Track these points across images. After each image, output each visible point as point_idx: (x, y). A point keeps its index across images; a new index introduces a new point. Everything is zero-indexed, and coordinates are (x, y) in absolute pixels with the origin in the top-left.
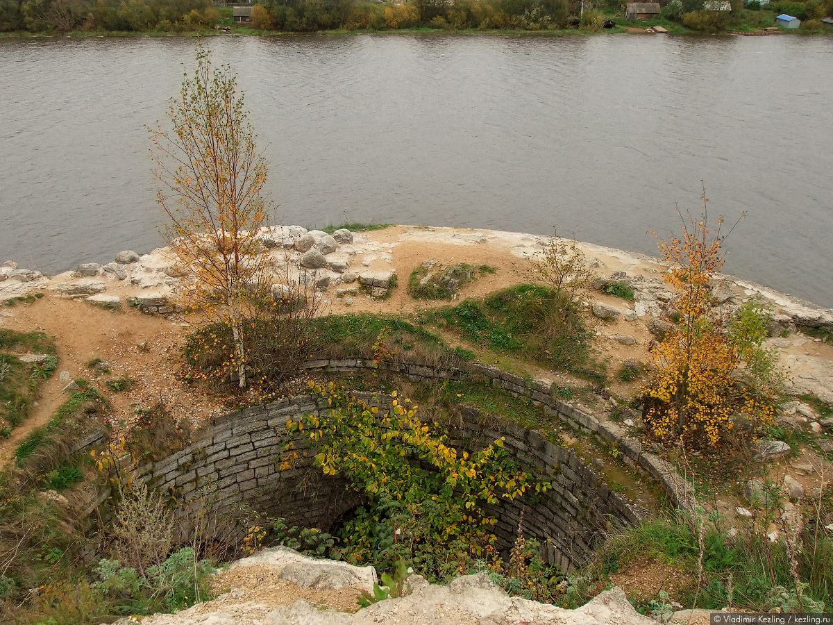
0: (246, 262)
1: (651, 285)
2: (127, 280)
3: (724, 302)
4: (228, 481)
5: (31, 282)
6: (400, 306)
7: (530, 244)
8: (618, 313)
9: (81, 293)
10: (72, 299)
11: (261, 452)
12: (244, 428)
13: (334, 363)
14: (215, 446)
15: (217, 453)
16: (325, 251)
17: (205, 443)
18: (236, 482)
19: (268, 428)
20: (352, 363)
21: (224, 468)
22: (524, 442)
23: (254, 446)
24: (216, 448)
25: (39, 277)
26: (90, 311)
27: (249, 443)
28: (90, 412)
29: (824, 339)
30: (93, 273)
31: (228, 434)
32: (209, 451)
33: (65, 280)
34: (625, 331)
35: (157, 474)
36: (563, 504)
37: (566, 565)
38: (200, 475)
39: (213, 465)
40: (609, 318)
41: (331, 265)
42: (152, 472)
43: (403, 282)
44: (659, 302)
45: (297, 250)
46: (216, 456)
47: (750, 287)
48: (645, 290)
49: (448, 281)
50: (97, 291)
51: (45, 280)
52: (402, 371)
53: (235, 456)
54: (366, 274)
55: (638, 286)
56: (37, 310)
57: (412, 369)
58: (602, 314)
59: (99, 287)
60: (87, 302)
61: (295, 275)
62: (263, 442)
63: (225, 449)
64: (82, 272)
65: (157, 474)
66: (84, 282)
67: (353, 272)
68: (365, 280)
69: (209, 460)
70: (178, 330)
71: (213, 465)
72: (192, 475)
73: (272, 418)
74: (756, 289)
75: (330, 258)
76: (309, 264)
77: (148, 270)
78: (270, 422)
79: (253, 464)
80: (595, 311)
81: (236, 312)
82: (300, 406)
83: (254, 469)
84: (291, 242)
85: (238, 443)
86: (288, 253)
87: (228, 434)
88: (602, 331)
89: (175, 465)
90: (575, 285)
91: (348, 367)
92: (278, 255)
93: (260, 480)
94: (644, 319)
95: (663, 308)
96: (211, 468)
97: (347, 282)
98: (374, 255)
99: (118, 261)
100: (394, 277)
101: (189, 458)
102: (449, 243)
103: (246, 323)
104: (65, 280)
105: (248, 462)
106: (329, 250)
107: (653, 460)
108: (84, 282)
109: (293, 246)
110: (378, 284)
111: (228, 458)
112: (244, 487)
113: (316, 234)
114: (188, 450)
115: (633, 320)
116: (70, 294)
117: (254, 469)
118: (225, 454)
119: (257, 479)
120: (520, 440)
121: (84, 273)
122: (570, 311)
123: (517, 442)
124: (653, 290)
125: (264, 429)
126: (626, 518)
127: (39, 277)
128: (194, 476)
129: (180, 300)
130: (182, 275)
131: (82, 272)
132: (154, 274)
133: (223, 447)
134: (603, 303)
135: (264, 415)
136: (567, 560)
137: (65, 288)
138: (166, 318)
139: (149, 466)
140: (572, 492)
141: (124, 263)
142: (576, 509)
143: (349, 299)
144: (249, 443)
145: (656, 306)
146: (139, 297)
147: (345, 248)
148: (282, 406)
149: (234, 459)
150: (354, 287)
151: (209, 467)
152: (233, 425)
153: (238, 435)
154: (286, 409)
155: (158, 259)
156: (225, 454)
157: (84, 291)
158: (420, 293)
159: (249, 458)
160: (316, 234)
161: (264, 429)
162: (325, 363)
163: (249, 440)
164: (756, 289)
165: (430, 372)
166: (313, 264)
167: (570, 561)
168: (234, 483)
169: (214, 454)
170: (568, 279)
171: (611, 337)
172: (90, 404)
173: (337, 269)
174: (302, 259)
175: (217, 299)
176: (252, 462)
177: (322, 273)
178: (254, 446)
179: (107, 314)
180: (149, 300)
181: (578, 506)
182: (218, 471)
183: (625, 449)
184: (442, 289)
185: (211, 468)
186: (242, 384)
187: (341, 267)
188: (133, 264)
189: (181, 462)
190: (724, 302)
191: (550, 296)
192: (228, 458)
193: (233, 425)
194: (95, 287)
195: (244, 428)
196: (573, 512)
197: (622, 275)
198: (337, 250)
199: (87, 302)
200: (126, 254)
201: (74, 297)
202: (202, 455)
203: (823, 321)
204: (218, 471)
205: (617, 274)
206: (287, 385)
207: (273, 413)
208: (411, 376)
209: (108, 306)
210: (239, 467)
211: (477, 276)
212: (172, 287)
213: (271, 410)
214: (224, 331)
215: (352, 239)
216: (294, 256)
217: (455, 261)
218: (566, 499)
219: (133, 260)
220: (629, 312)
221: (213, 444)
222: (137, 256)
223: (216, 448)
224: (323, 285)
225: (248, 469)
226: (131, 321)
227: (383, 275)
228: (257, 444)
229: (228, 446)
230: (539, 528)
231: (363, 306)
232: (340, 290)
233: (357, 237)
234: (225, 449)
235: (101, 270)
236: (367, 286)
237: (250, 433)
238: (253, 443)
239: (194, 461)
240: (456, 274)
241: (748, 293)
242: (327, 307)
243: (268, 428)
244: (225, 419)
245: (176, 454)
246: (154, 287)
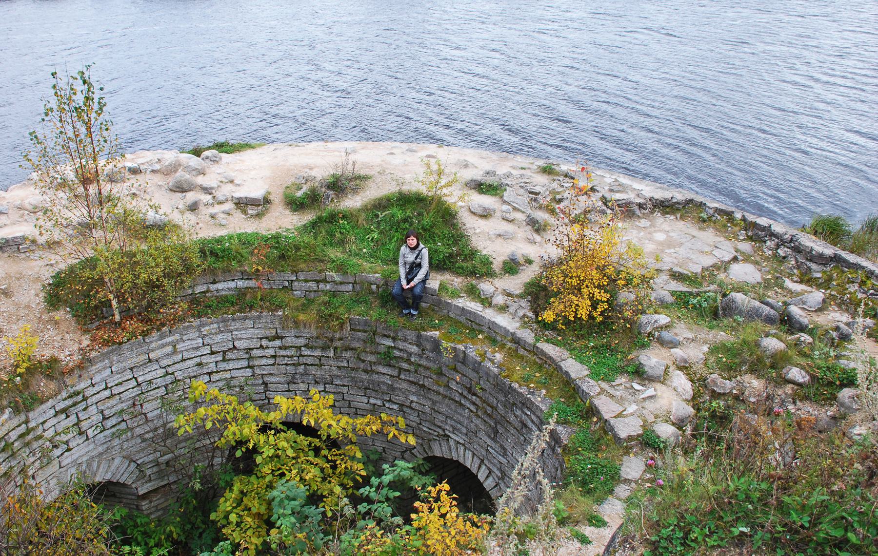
0: (118, 189)
4: (113, 421)
6: (283, 222)
12: (124, 364)
16: (194, 173)
18: (123, 420)
21: (108, 408)
22: (417, 345)
23: (137, 381)
24: (97, 388)
26: (434, 154)
29: (678, 216)
36: (463, 402)
37: (470, 458)
38: (82, 418)
39: (94, 407)
43: (277, 198)
46: (97, 396)
47: (607, 175)
53: (119, 394)
55: (509, 183)
58: (479, 211)
62: (147, 376)
67: (227, 191)
69: (89, 401)
70: (42, 268)
71: (94, 407)
73: (153, 351)
75: (200, 180)
76: (178, 187)
78: (152, 355)
81: (107, 242)
89: (52, 412)
93: (148, 415)
96: (93, 410)
98: (255, 172)
107: (550, 349)
118: (107, 393)
123: (410, 346)
124: (523, 185)
126: (528, 408)
128: (76, 420)
133: (104, 386)
136: (470, 453)
149: (118, 397)
151: (90, 409)
156: (107, 393)
159: (134, 395)
163: (131, 376)
167: (474, 454)
168: (121, 422)
177: (191, 197)
178: (137, 381)
183: (516, 341)
187: (212, 188)
195: (124, 364)
203: (674, 200)
207: (153, 345)
213: (151, 342)
215: (221, 159)
223: (97, 388)
227: (257, 193)
228: (140, 379)
229: (109, 385)
230: (440, 427)
231: (241, 225)
236: (242, 204)
237: (131, 369)
238: (136, 379)
242: (200, 229)
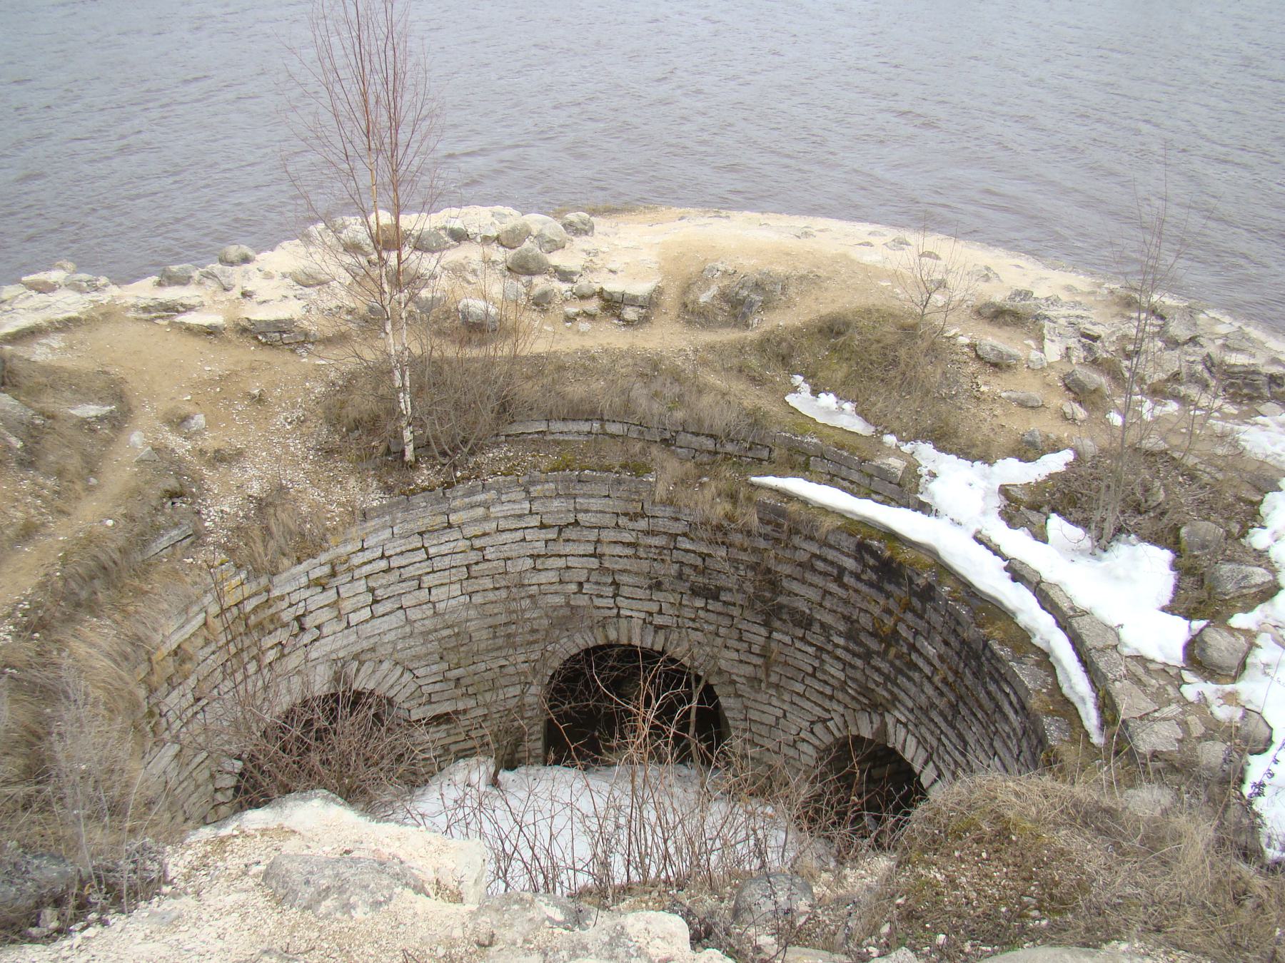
1: (1073, 312)
2: (236, 293)
3: (1185, 343)
5: (95, 294)
7: (884, 240)
8: (1017, 359)
9: (166, 311)
10: (152, 320)
11: (438, 564)
13: (557, 426)
14: (367, 553)
15: (370, 562)
16: (548, 246)
17: (350, 548)
19: (450, 526)
20: (585, 427)
22: (856, 559)
23: (427, 553)
24: (368, 555)
25: (105, 286)
27: (419, 549)
28: (173, 495)
30: (183, 281)
31: (387, 534)
32: (356, 560)
33: (145, 291)
34: (1031, 388)
35: (276, 593)
37: (913, 748)
38: (343, 595)
39: (363, 582)
40: (999, 365)
41: (557, 269)
42: (268, 591)
43: (670, 300)
44: (1083, 340)
45: (502, 245)
47: (1227, 319)
48: (1063, 321)
49: (745, 298)
50: (189, 308)
51: (114, 290)
52: (664, 441)
54: (614, 286)
56: (106, 333)
57: (684, 439)
58: (992, 357)
59: (194, 301)
60: (172, 324)
61: (496, 286)
62: (443, 547)
63: (383, 557)
64: (169, 278)
65: (276, 593)
66: (171, 294)
67: (583, 283)
68: (610, 294)
69: (357, 574)
71: (363, 582)
72: (331, 595)
74: (1237, 324)
75: (556, 259)
77: (268, 276)
78: (581, 517)
79: (428, 581)
80: (980, 352)
82: (499, 492)
83: (430, 589)
84: (493, 233)
85: (404, 548)
86: (486, 249)
87: (387, 534)
88: (990, 385)
89: (304, 580)
90: (947, 308)
91: (579, 433)
92: (470, 254)
94: (1059, 367)
95: (1089, 349)
97: (583, 297)
98: (630, 253)
99: (224, 261)
100: (659, 291)
101: (326, 570)
102: (747, 239)
103: (415, 363)
104: (145, 291)
105: (419, 578)
106: (556, 246)
108: (171, 294)
109: (497, 239)
110: (632, 301)
111: (389, 570)
112: (414, 614)
113: (536, 221)
114: (323, 557)
115: (1040, 370)
116: (150, 312)
117: (430, 589)
118: (383, 564)
119: (434, 603)
120: (848, 556)
121: (169, 280)
122: (938, 349)
123: (845, 559)
124: (1072, 320)
125: (445, 528)
127: (105, 286)
129: (316, 325)
130: (321, 283)
131: (169, 278)
132: (276, 281)
133: (379, 554)
134: (994, 340)
135: (444, 507)
137: (142, 303)
138: (293, 351)
139: (264, 580)
140: (926, 639)
141: (232, 264)
142: (932, 665)
143: (584, 325)
144: (419, 549)
145: (1078, 346)
146: (253, 318)
147: (581, 242)
148: (471, 493)
150: (593, 305)
152: (393, 520)
153: (401, 537)
154: (480, 497)
155: (286, 257)
156: (383, 564)
157: (171, 309)
158: (694, 315)
160: (536, 221)
161: (445, 528)
162: (543, 427)
163: (419, 545)
164: (1237, 324)
165: (709, 444)
166: (522, 268)
169: (365, 564)
170: (938, 299)
171: (1004, 395)
172: (172, 483)
173: (565, 276)
174: (510, 260)
175: (373, 321)
176: (424, 578)
177: (541, 283)
178: (427, 553)
179: (197, 344)
180: (267, 323)
181: (936, 662)
182: (371, 590)
184: (737, 306)
185: (361, 586)
186: (409, 455)
187: (573, 273)
188: (246, 266)
189: (313, 575)
190: (1185, 343)
191: (909, 331)
192: (389, 570)
193: (393, 520)
194: (186, 302)
196: (927, 670)
197: (1027, 295)
198: (567, 245)
199: (172, 324)
200: (233, 251)
201: (156, 318)
202: (346, 566)
204: (371, 590)
205: (1018, 293)
206: (480, 459)
207: (457, 503)
208: (679, 450)
209: (211, 332)
210: (403, 585)
211: (792, 291)
212: (302, 303)
213: (454, 498)
214: (381, 373)
215: (592, 228)
216: (499, 254)
217: (750, 265)
218: (917, 651)
219: (246, 260)
220: (1035, 355)
221: (363, 549)
222: (251, 253)
223: (368, 555)
224: (541, 302)
225: (420, 588)
226: (249, 353)
227: (641, 288)
228: (432, 551)
229: (387, 554)
231: (607, 338)
232: (572, 310)
233: (600, 224)
234: (383, 557)
235: (196, 275)
236: (612, 305)
237: (421, 534)
239: (333, 574)
240: (758, 286)
241: (1222, 329)
242: (544, 339)
243: (450, 526)
244: (381, 511)
245: (305, 564)
246: (275, 302)
